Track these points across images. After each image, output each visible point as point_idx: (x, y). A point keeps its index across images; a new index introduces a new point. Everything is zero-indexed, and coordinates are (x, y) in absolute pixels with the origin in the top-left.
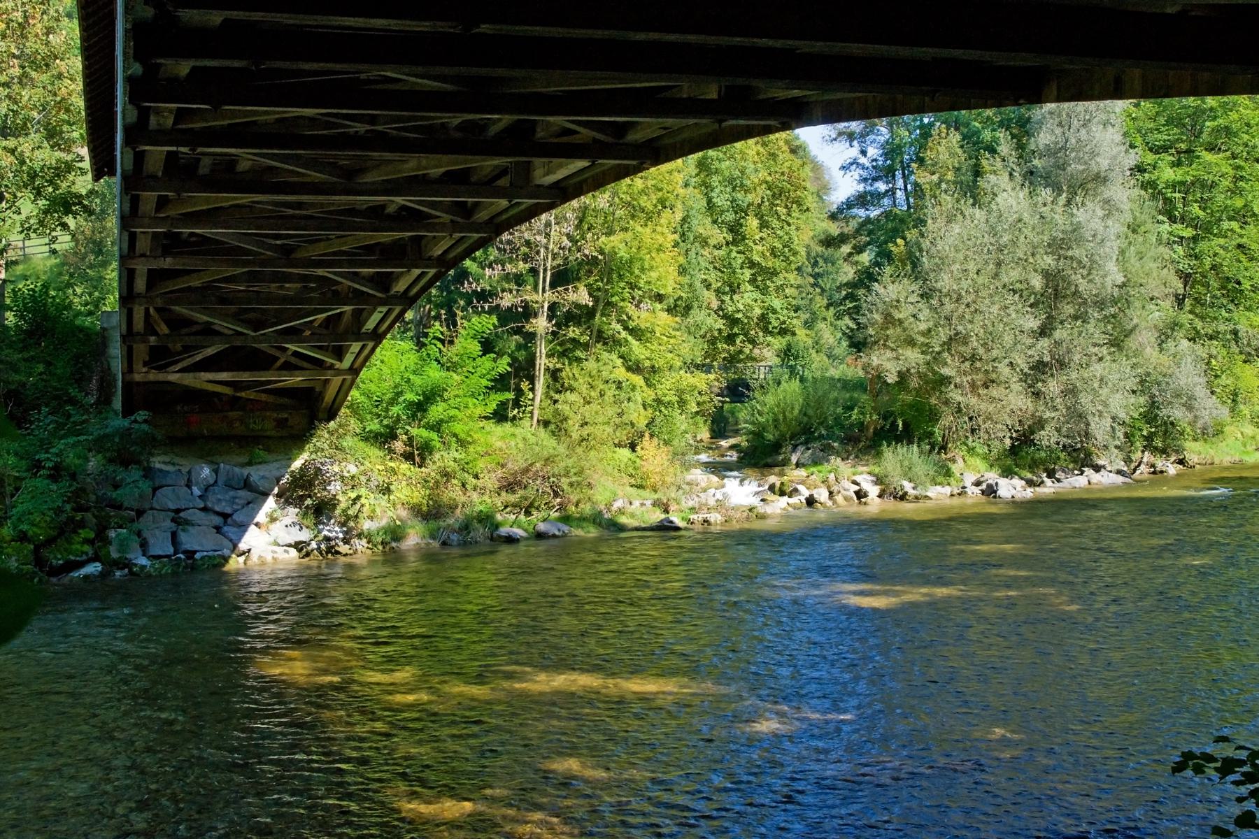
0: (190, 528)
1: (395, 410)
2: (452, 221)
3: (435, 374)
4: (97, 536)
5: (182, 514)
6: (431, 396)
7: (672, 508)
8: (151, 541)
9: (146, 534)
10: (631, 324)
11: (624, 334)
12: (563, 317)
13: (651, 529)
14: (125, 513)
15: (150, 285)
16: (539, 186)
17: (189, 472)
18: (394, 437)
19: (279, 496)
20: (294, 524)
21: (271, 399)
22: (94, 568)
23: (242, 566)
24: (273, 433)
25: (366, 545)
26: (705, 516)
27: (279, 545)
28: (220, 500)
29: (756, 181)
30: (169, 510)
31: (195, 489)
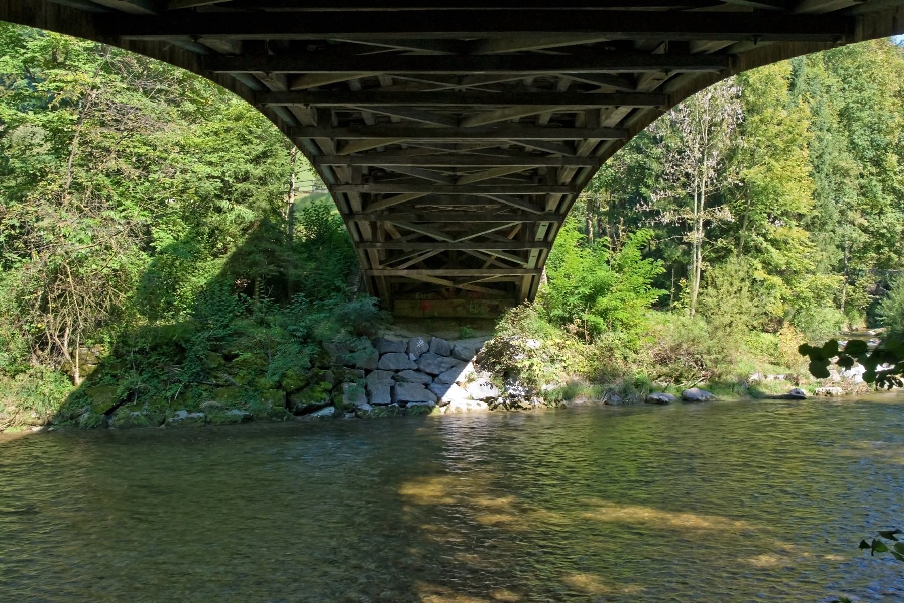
0: (405, 384)
1: (572, 300)
2: (563, 156)
3: (603, 273)
4: (334, 387)
5: (400, 374)
6: (600, 290)
7: (801, 382)
8: (374, 392)
9: (369, 388)
10: (770, 237)
11: (765, 244)
12: (711, 234)
13: (781, 398)
14: (355, 371)
15: (364, 206)
16: (606, 127)
17: (408, 343)
18: (571, 321)
19: (477, 362)
20: (487, 384)
21: (484, 290)
22: (329, 411)
23: (443, 413)
24: (487, 316)
25: (543, 402)
26: (828, 389)
27: (473, 399)
28: (430, 364)
29: (894, 125)
30: (390, 370)
31: (411, 355)
